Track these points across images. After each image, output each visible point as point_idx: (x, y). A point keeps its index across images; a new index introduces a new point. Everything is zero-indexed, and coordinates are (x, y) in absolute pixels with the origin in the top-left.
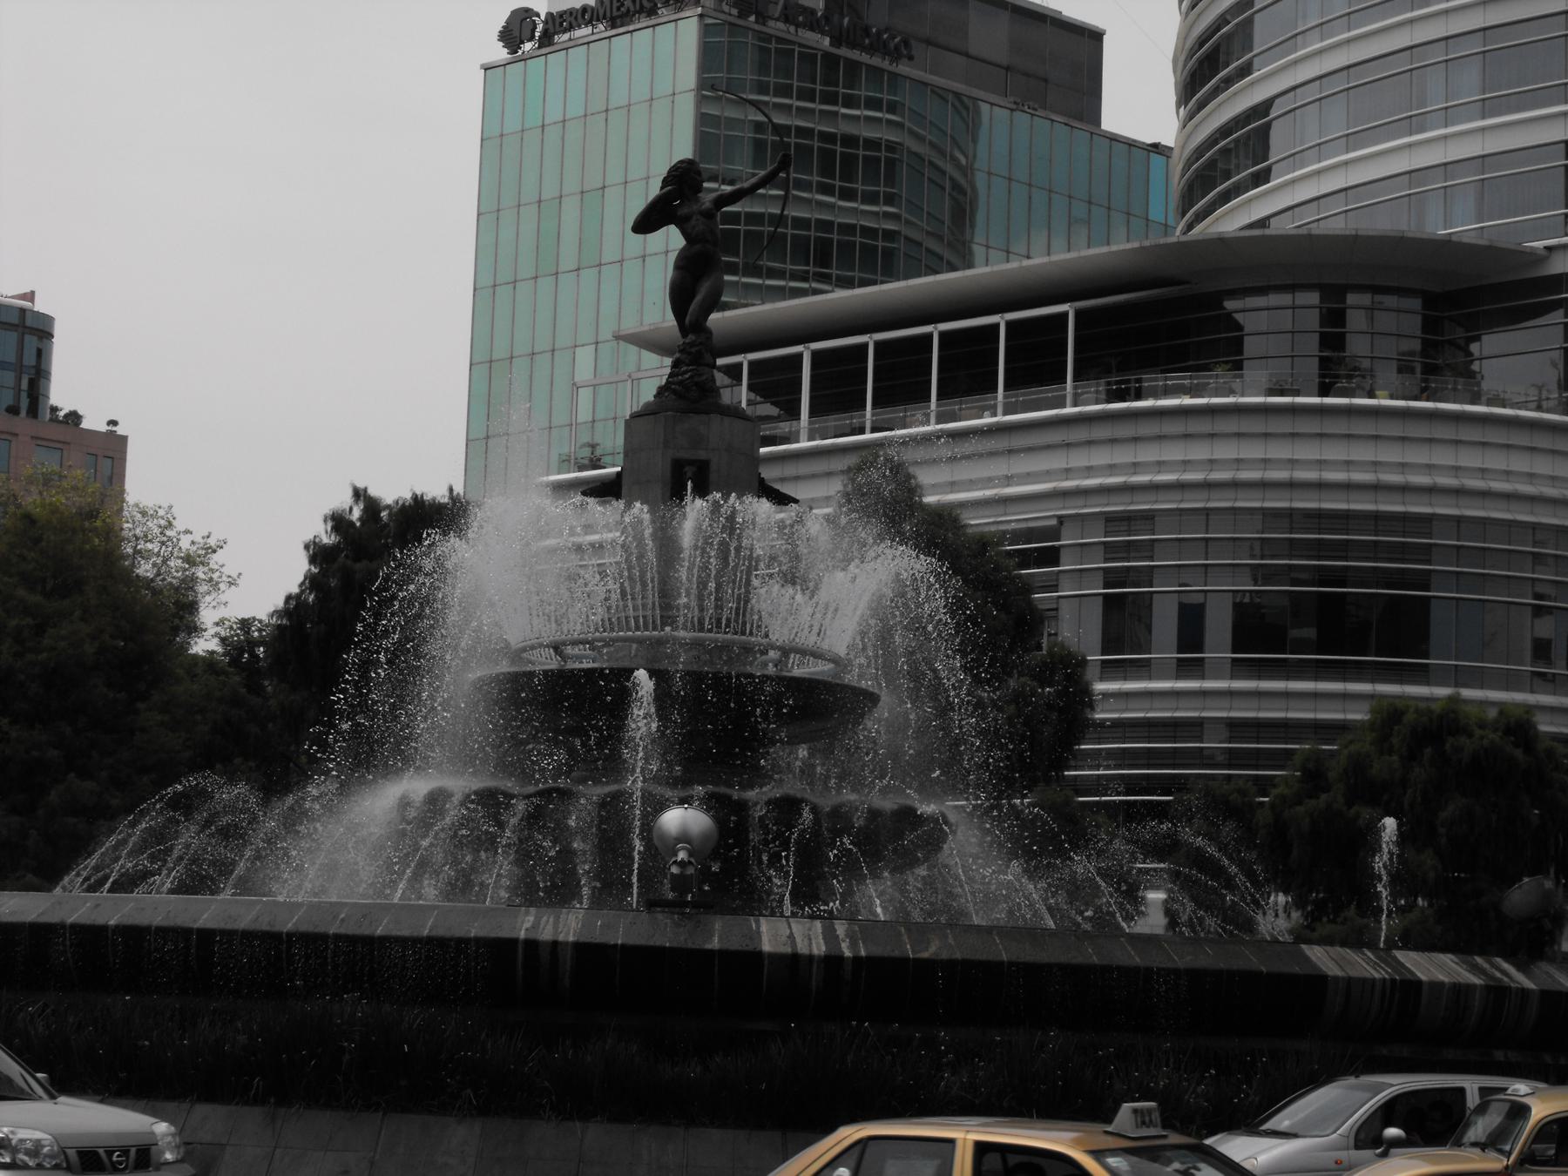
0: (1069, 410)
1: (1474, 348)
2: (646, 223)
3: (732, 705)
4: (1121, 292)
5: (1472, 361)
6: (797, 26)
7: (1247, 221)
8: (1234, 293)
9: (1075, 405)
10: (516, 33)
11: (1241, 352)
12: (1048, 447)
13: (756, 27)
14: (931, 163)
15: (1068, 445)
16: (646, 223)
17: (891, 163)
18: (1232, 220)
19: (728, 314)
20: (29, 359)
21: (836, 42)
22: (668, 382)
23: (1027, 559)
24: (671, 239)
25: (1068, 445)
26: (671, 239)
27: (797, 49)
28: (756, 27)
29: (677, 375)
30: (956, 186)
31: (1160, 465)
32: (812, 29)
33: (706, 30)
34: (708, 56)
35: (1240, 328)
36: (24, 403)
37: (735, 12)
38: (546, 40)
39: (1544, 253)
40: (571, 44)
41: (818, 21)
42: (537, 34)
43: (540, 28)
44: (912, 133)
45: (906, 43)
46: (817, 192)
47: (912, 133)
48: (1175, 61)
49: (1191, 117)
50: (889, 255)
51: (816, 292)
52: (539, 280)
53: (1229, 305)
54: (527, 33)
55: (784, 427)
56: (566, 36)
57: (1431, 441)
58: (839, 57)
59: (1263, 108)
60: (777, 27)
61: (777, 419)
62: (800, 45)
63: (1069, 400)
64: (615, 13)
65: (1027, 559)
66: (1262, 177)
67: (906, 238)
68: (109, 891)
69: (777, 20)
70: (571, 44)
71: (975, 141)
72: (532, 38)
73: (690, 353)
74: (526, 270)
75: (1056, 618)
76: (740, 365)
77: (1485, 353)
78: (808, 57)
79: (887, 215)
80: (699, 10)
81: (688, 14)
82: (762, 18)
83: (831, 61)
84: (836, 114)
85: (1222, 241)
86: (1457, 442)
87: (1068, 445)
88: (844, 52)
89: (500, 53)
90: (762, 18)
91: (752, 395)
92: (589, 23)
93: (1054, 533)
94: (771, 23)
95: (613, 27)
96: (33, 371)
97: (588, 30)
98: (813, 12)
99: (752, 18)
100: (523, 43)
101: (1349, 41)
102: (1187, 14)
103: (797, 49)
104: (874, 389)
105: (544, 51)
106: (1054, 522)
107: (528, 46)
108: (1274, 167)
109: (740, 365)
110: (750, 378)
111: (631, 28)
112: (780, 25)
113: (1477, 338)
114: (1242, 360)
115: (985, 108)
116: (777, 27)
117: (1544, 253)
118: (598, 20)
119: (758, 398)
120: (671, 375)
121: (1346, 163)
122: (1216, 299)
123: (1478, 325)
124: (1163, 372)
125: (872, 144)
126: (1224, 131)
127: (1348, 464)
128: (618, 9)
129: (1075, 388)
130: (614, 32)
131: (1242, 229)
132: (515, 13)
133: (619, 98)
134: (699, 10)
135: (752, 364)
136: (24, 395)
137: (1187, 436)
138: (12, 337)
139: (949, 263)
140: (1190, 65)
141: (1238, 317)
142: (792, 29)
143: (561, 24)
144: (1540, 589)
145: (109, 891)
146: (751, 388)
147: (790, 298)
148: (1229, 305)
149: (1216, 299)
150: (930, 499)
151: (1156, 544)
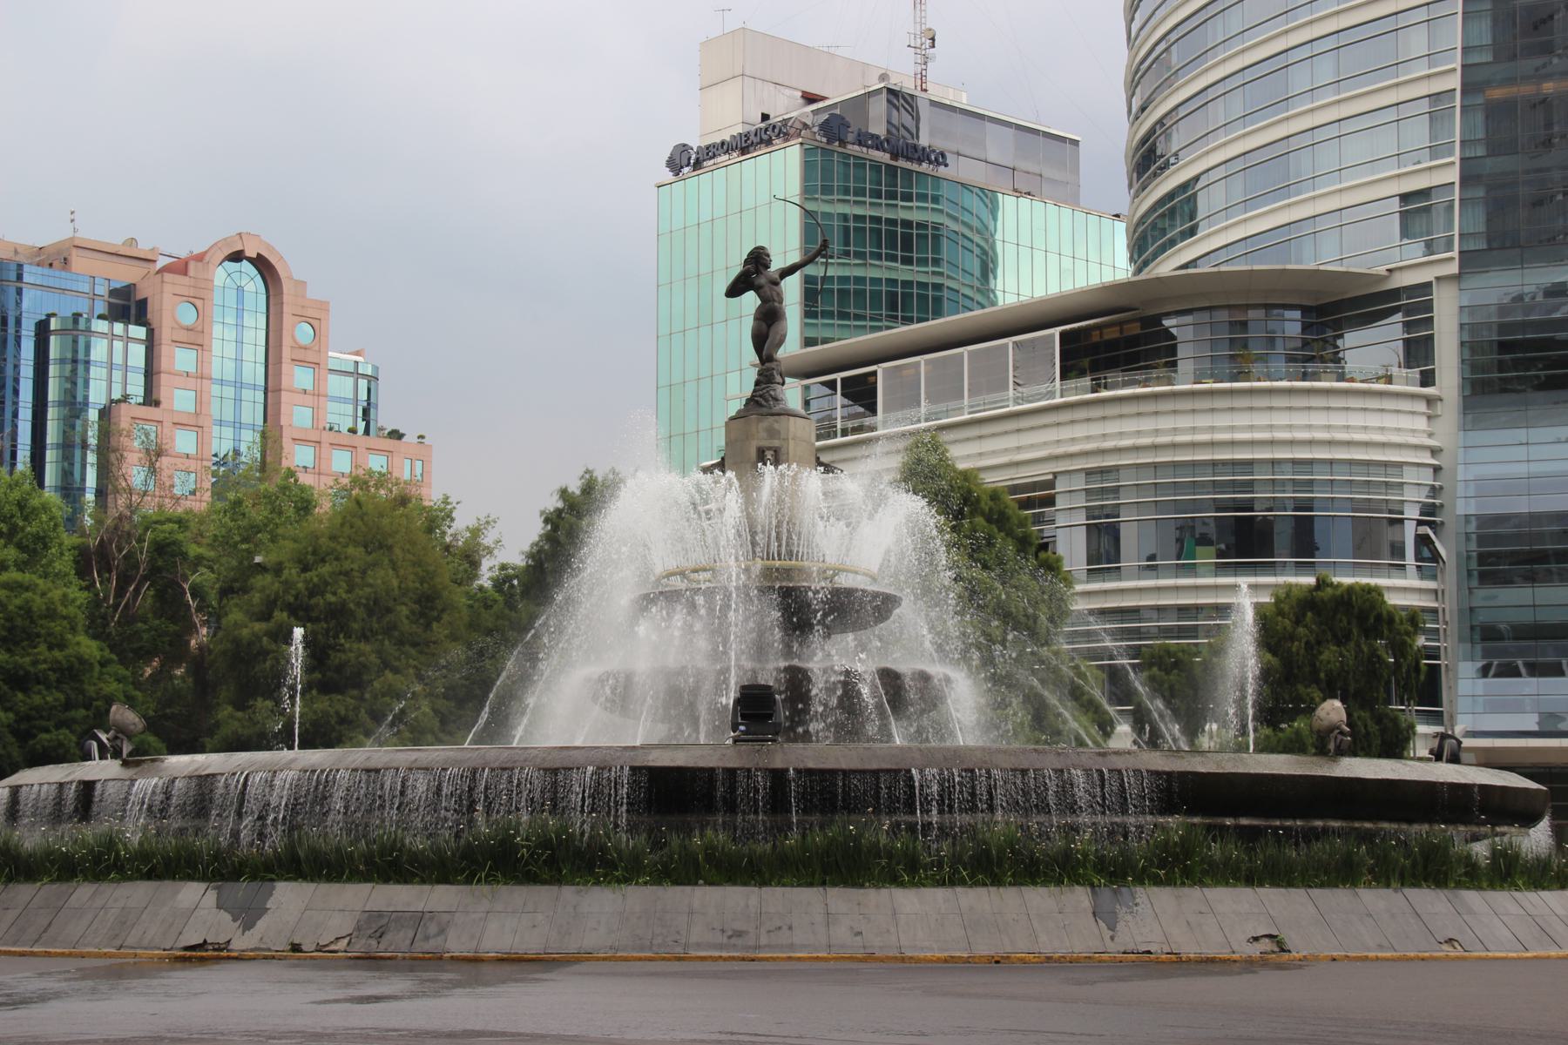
0: (1058, 400)
1: (1339, 342)
2: (735, 290)
3: (795, 620)
4: (1080, 321)
5: (1338, 352)
6: (868, 147)
7: (1178, 264)
8: (1168, 315)
9: (1062, 396)
10: (678, 161)
11: (1175, 354)
12: (1045, 426)
13: (840, 150)
14: (963, 235)
15: (1058, 424)
16: (735, 290)
17: (936, 238)
18: (1166, 266)
19: (826, 346)
20: (363, 396)
21: (895, 156)
22: (753, 396)
23: (1027, 504)
24: (750, 300)
25: (1058, 424)
26: (750, 300)
27: (868, 162)
28: (840, 150)
29: (759, 390)
30: (985, 252)
31: (1121, 435)
32: (878, 149)
33: (807, 152)
34: (808, 167)
35: (1173, 337)
36: (361, 426)
37: (824, 140)
38: (698, 165)
39: (1386, 273)
40: (715, 167)
41: (881, 143)
42: (692, 161)
43: (694, 157)
44: (949, 215)
45: (943, 155)
46: (886, 260)
47: (949, 215)
48: (1126, 157)
49: (1136, 196)
50: (938, 301)
51: (888, 328)
52: (729, 322)
53: (1167, 323)
54: (685, 162)
55: (868, 421)
56: (712, 162)
57: (1271, 408)
58: (896, 167)
59: (1184, 187)
60: (854, 149)
61: (863, 416)
62: (870, 160)
63: (1058, 394)
64: (744, 145)
65: (1027, 504)
66: (1192, 232)
67: (948, 287)
68: (474, 742)
69: (853, 144)
70: (715, 167)
71: (995, 219)
72: (688, 165)
73: (766, 376)
74: (692, 323)
75: (1055, 541)
76: (835, 381)
77: (1347, 346)
78: (876, 167)
79: (934, 273)
80: (800, 140)
81: (792, 143)
82: (843, 143)
83: (892, 170)
84: (896, 206)
85: (1160, 280)
86: (1328, 409)
87: (1058, 424)
88: (902, 163)
89: (668, 176)
90: (843, 143)
91: (846, 401)
92: (727, 152)
93: (1050, 484)
94: (850, 147)
95: (743, 154)
96: (365, 404)
97: (727, 157)
98: (878, 137)
99: (837, 143)
100: (682, 167)
101: (1244, 135)
102: (1133, 123)
103: (868, 162)
104: (969, 384)
105: (696, 173)
106: (1050, 477)
107: (686, 170)
108: (1201, 223)
109: (835, 381)
110: (842, 389)
111: (755, 154)
112: (856, 147)
113: (1341, 336)
114: (1175, 362)
115: (1000, 195)
116: (854, 149)
117: (1386, 273)
118: (732, 150)
119: (851, 403)
120: (754, 391)
121: (1245, 220)
122: (1156, 320)
123: (1340, 326)
124: (1123, 371)
125: (921, 225)
126: (1153, 208)
127: (1251, 428)
128: (746, 141)
129: (1061, 385)
130: (744, 157)
131: (1175, 269)
132: (676, 147)
133: (748, 203)
134: (800, 140)
135: (843, 380)
136: (360, 420)
137: (1139, 414)
138: (350, 380)
139: (978, 303)
140: (1135, 160)
141: (1174, 331)
142: (865, 149)
143: (708, 154)
144: (1391, 507)
145: (474, 742)
146: (843, 395)
147: (870, 333)
148: (1167, 323)
149: (1156, 320)
150: (961, 466)
151: (1121, 489)
